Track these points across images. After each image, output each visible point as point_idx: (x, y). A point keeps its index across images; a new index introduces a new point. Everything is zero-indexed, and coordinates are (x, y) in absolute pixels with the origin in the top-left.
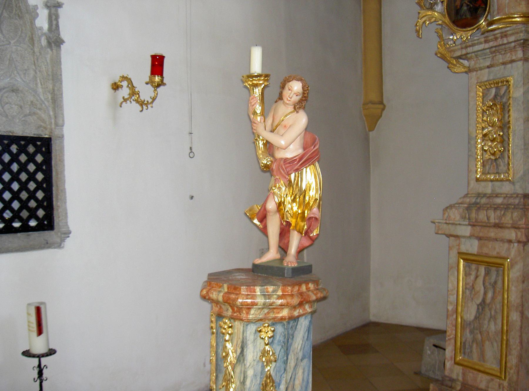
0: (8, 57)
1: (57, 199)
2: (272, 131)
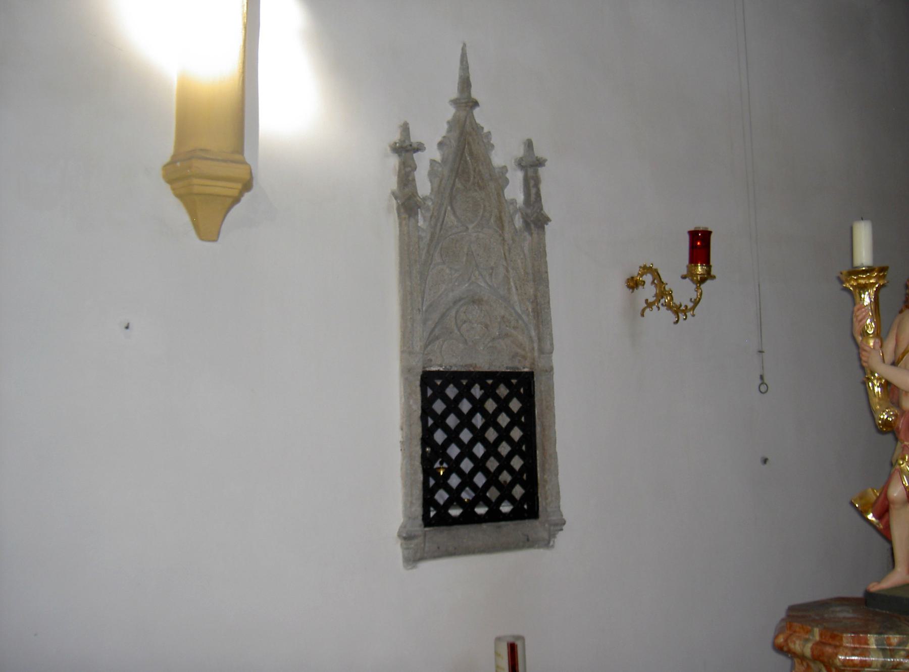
0: (465, 250)
1: (543, 470)
2: (894, 364)
